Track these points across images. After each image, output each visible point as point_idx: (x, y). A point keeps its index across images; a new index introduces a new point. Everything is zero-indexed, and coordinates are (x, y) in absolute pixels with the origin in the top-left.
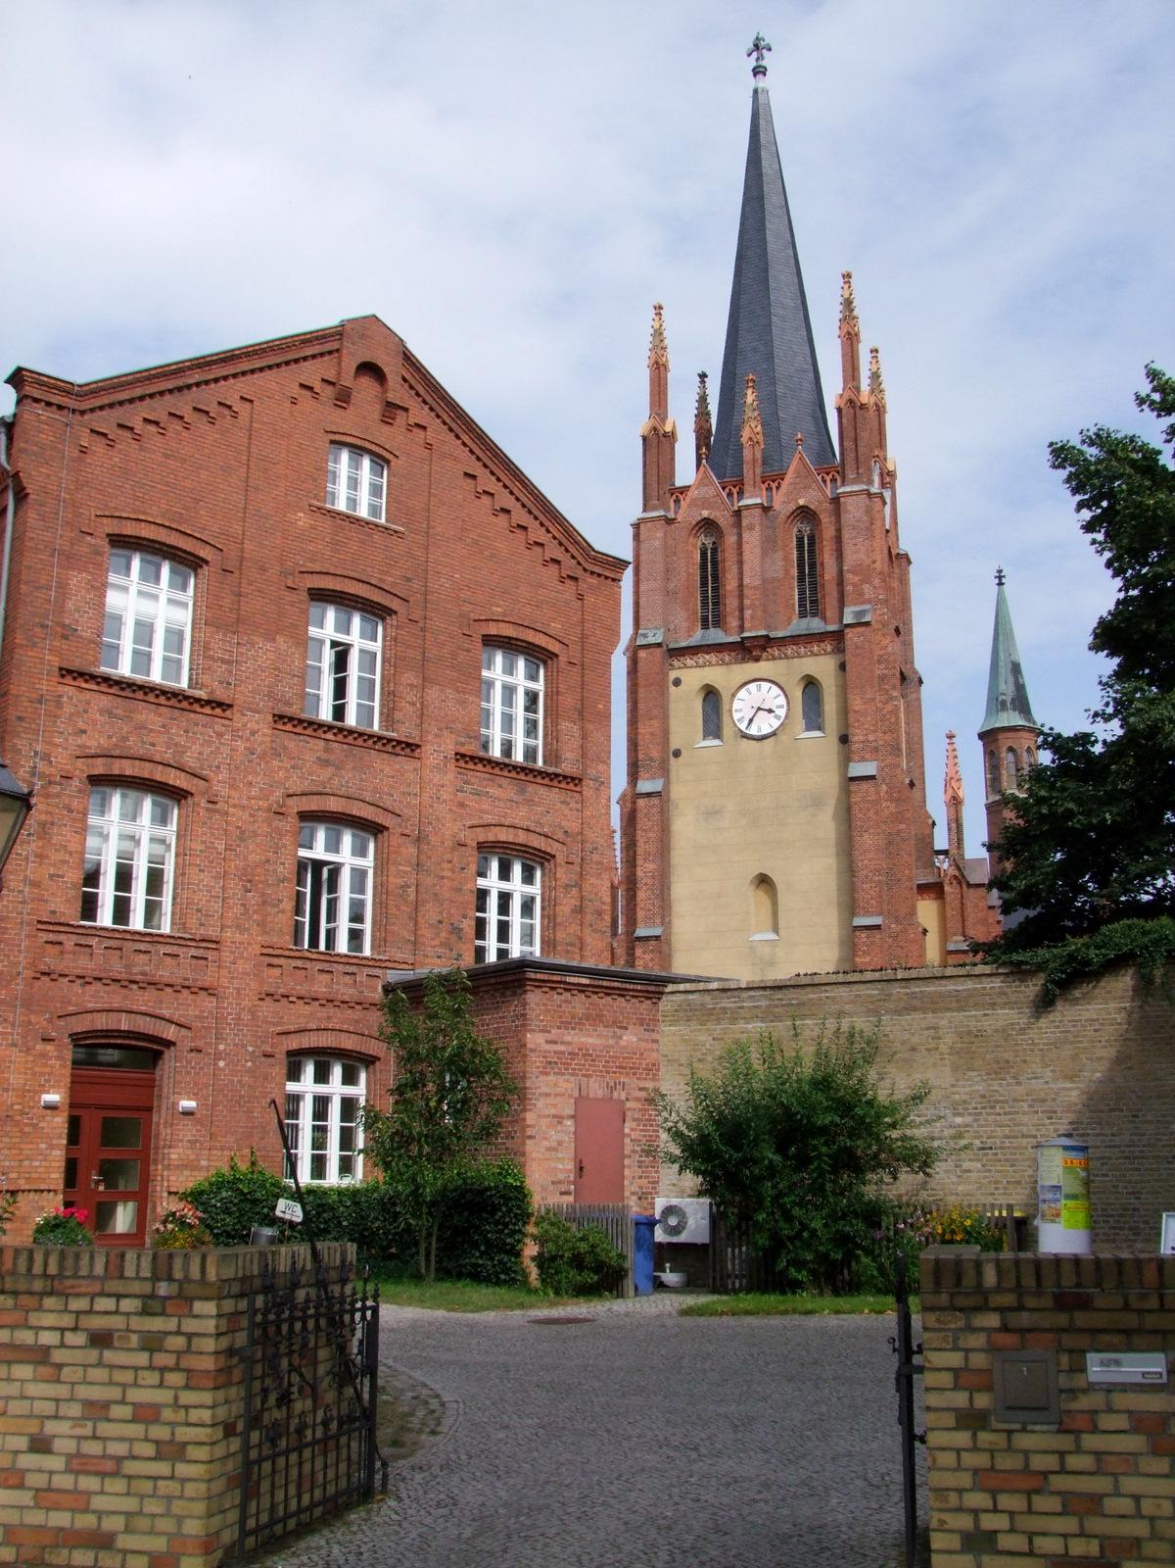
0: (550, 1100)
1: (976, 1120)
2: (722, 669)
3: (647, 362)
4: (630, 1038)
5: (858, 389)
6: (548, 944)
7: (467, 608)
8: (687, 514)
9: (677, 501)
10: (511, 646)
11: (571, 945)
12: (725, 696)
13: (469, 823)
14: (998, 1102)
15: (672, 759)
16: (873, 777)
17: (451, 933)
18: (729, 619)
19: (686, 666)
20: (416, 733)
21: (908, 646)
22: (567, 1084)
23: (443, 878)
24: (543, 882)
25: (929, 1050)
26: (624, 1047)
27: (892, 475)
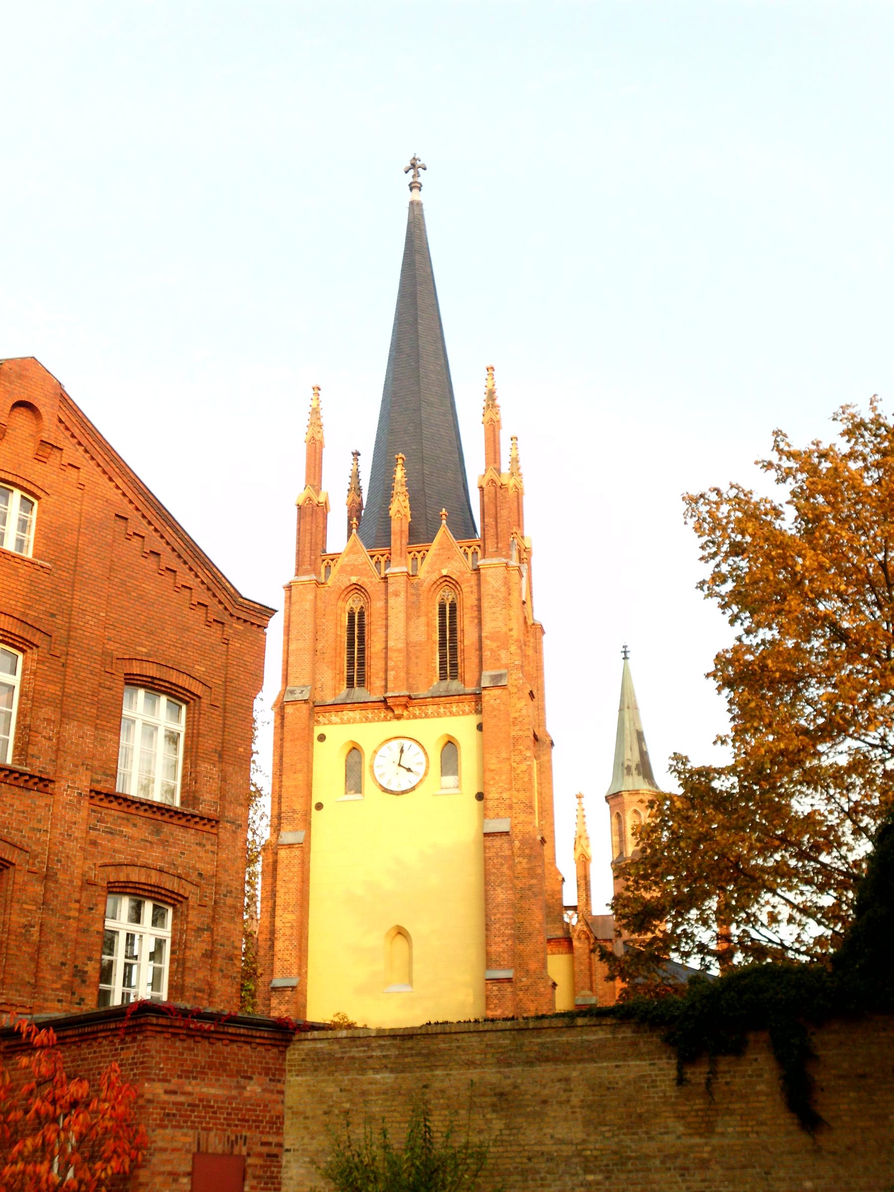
0: (165, 1156)
1: (607, 1178)
3: (305, 437)
4: (253, 1089)
5: (499, 471)
6: (173, 988)
7: (110, 646)
8: (336, 579)
9: (328, 567)
10: (154, 686)
11: (200, 990)
13: (100, 862)
14: (629, 1158)
16: (507, 833)
17: (74, 976)
18: (373, 679)
19: (330, 723)
20: (50, 769)
21: (540, 709)
22: (185, 1138)
23: (69, 918)
24: (173, 924)
25: (560, 1103)
26: (249, 1099)
27: (527, 550)
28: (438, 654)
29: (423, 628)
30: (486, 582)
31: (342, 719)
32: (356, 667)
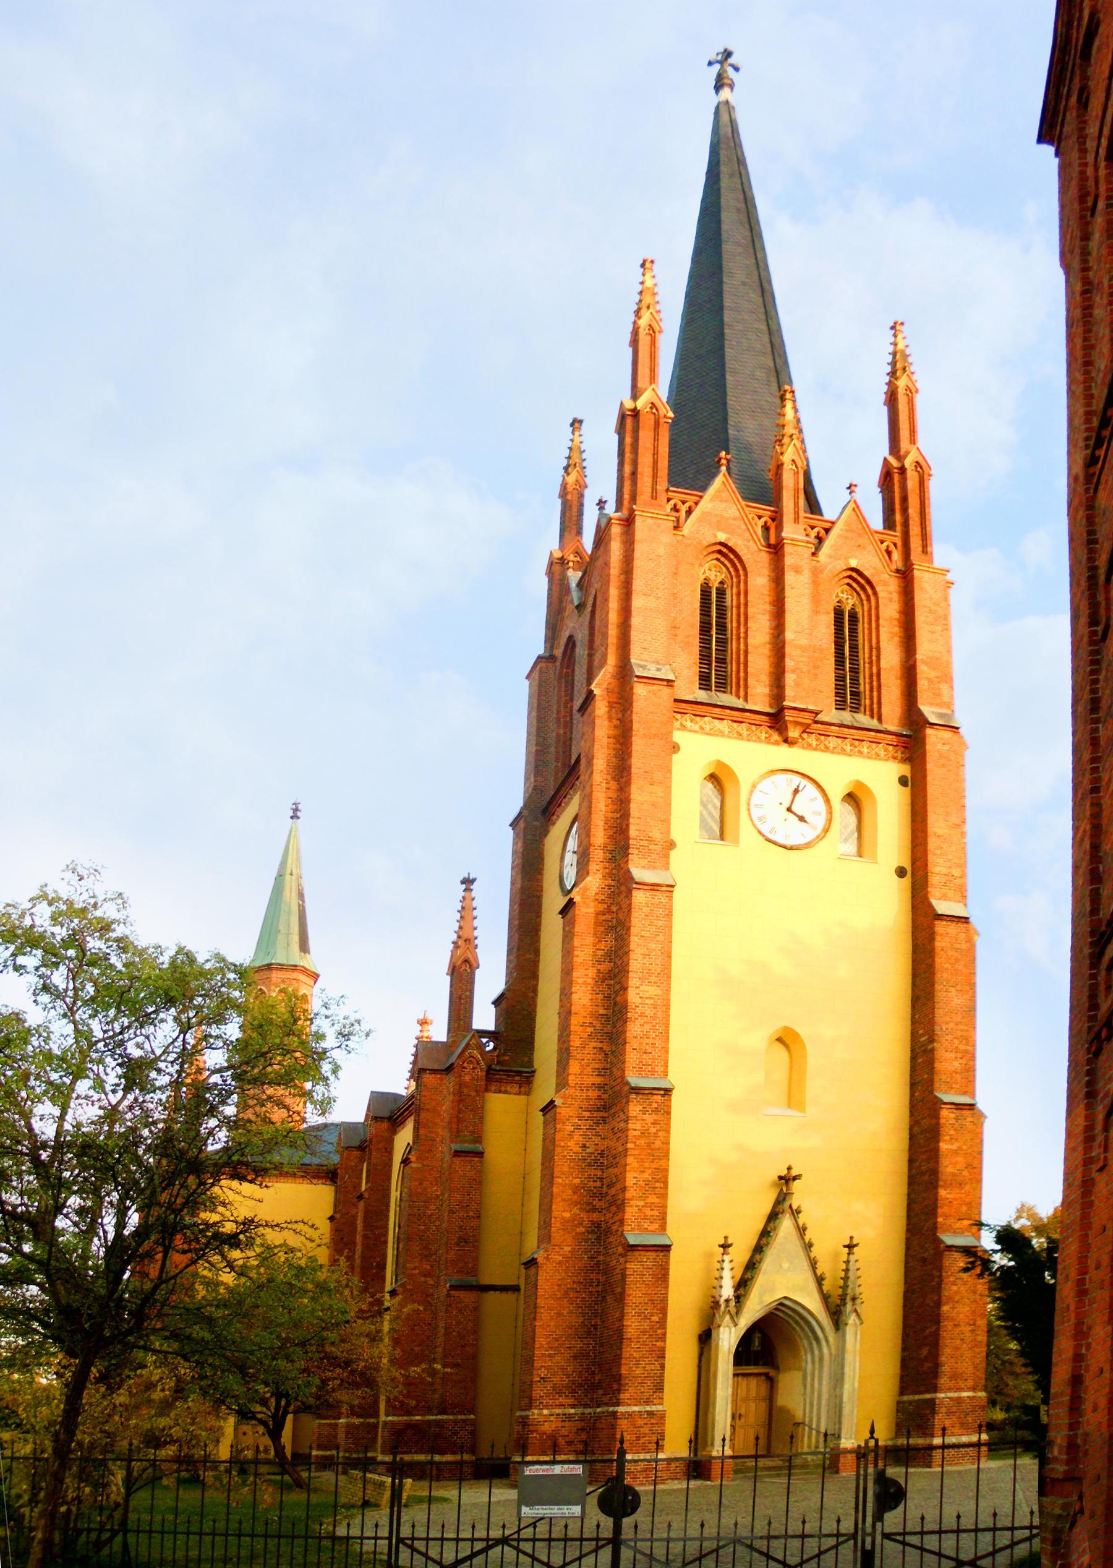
30: (922, 589)
31: (702, 728)
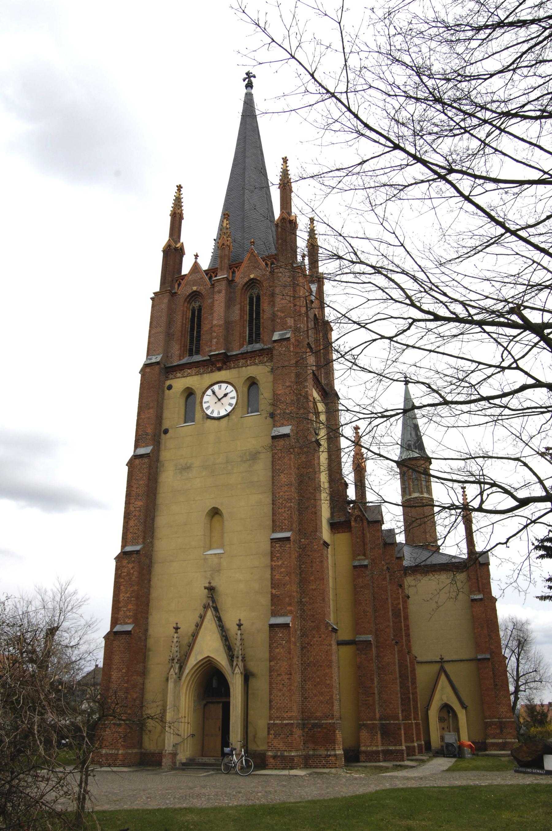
2: (195, 378)
8: (184, 291)
12: (198, 393)
15: (163, 435)
28: (247, 328)
29: (238, 312)
32: (195, 343)
